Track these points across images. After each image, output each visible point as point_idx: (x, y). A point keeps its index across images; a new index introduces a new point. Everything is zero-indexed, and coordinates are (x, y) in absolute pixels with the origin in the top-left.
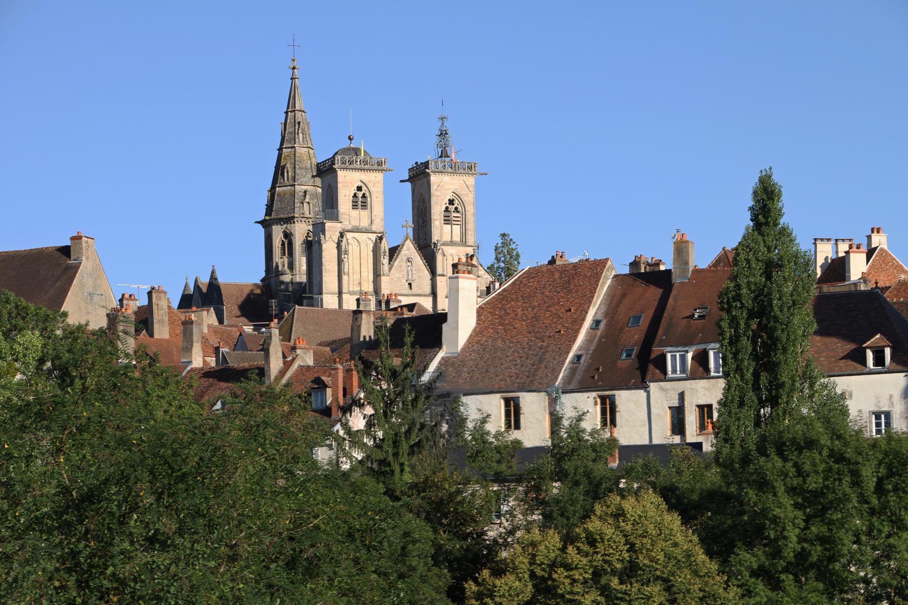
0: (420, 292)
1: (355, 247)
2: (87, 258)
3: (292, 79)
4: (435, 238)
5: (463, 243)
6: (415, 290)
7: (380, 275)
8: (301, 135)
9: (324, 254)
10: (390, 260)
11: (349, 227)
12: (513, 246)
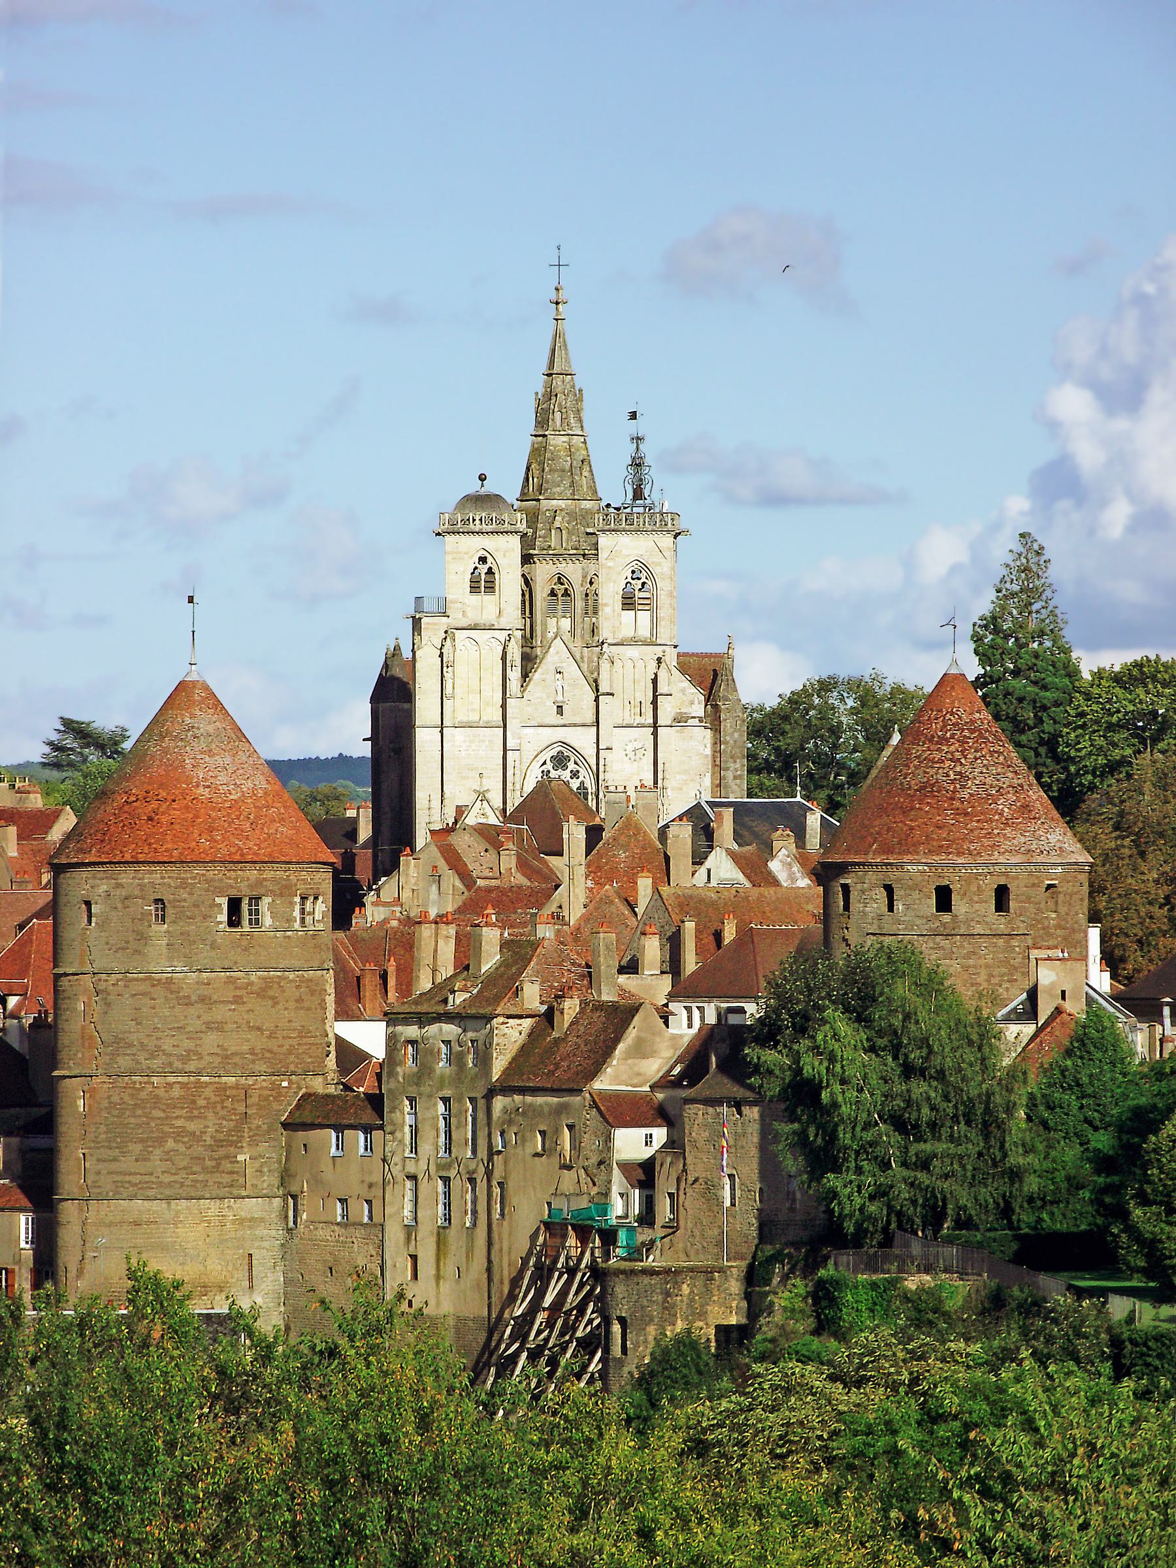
0: (578, 721)
6: (568, 718)
8: (558, 415)
10: (525, 676)
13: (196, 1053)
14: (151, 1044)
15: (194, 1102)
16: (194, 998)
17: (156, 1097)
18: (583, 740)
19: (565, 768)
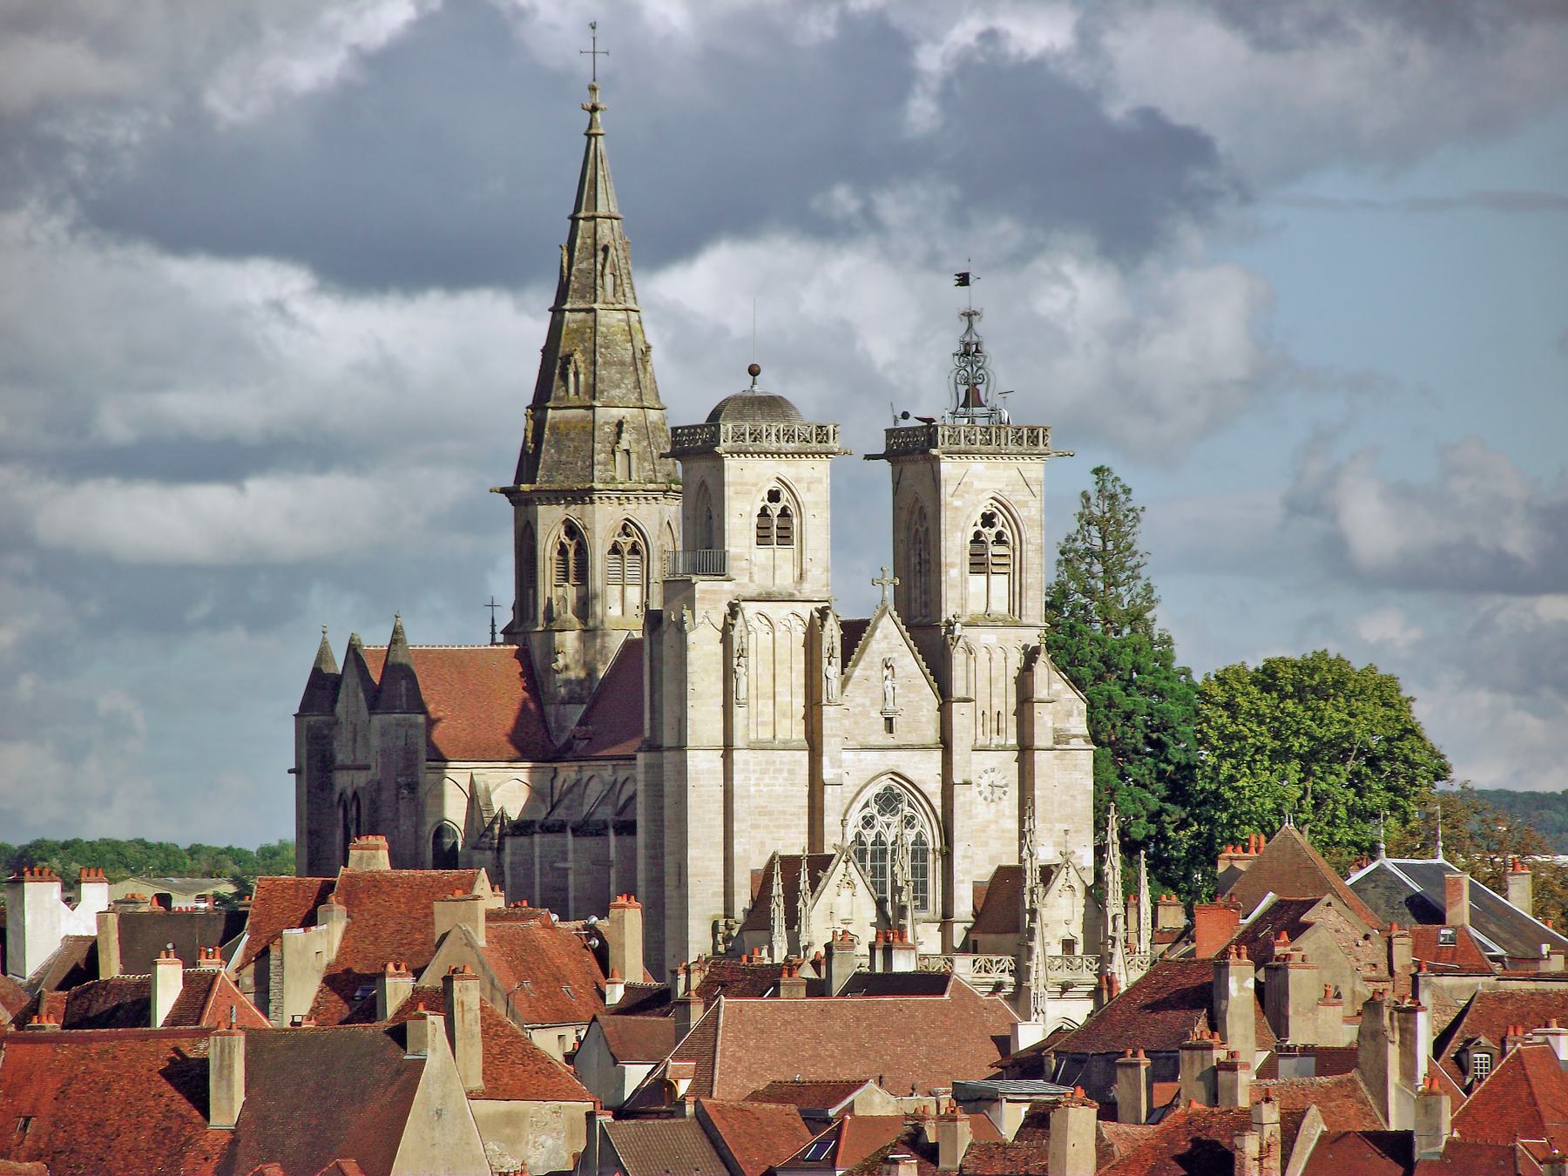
1: (762, 635)
2: (434, 1050)
3: (589, 136)
4: (949, 610)
6: (900, 736)
7: (819, 704)
8: (609, 279)
9: (689, 669)
10: (844, 665)
11: (752, 590)
18: (925, 770)
19: (894, 811)
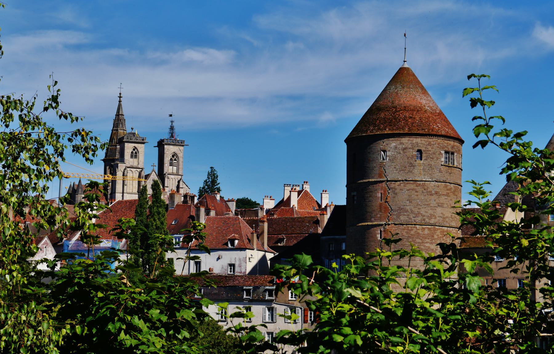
5: (177, 174)
7: (115, 193)
11: (129, 166)
12: (215, 172)
13: (434, 216)
14: (416, 210)
15: (433, 236)
16: (433, 192)
17: (418, 233)
